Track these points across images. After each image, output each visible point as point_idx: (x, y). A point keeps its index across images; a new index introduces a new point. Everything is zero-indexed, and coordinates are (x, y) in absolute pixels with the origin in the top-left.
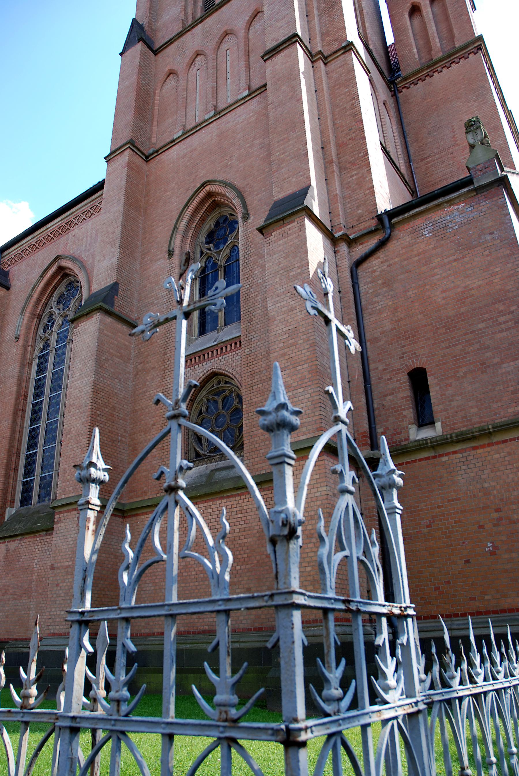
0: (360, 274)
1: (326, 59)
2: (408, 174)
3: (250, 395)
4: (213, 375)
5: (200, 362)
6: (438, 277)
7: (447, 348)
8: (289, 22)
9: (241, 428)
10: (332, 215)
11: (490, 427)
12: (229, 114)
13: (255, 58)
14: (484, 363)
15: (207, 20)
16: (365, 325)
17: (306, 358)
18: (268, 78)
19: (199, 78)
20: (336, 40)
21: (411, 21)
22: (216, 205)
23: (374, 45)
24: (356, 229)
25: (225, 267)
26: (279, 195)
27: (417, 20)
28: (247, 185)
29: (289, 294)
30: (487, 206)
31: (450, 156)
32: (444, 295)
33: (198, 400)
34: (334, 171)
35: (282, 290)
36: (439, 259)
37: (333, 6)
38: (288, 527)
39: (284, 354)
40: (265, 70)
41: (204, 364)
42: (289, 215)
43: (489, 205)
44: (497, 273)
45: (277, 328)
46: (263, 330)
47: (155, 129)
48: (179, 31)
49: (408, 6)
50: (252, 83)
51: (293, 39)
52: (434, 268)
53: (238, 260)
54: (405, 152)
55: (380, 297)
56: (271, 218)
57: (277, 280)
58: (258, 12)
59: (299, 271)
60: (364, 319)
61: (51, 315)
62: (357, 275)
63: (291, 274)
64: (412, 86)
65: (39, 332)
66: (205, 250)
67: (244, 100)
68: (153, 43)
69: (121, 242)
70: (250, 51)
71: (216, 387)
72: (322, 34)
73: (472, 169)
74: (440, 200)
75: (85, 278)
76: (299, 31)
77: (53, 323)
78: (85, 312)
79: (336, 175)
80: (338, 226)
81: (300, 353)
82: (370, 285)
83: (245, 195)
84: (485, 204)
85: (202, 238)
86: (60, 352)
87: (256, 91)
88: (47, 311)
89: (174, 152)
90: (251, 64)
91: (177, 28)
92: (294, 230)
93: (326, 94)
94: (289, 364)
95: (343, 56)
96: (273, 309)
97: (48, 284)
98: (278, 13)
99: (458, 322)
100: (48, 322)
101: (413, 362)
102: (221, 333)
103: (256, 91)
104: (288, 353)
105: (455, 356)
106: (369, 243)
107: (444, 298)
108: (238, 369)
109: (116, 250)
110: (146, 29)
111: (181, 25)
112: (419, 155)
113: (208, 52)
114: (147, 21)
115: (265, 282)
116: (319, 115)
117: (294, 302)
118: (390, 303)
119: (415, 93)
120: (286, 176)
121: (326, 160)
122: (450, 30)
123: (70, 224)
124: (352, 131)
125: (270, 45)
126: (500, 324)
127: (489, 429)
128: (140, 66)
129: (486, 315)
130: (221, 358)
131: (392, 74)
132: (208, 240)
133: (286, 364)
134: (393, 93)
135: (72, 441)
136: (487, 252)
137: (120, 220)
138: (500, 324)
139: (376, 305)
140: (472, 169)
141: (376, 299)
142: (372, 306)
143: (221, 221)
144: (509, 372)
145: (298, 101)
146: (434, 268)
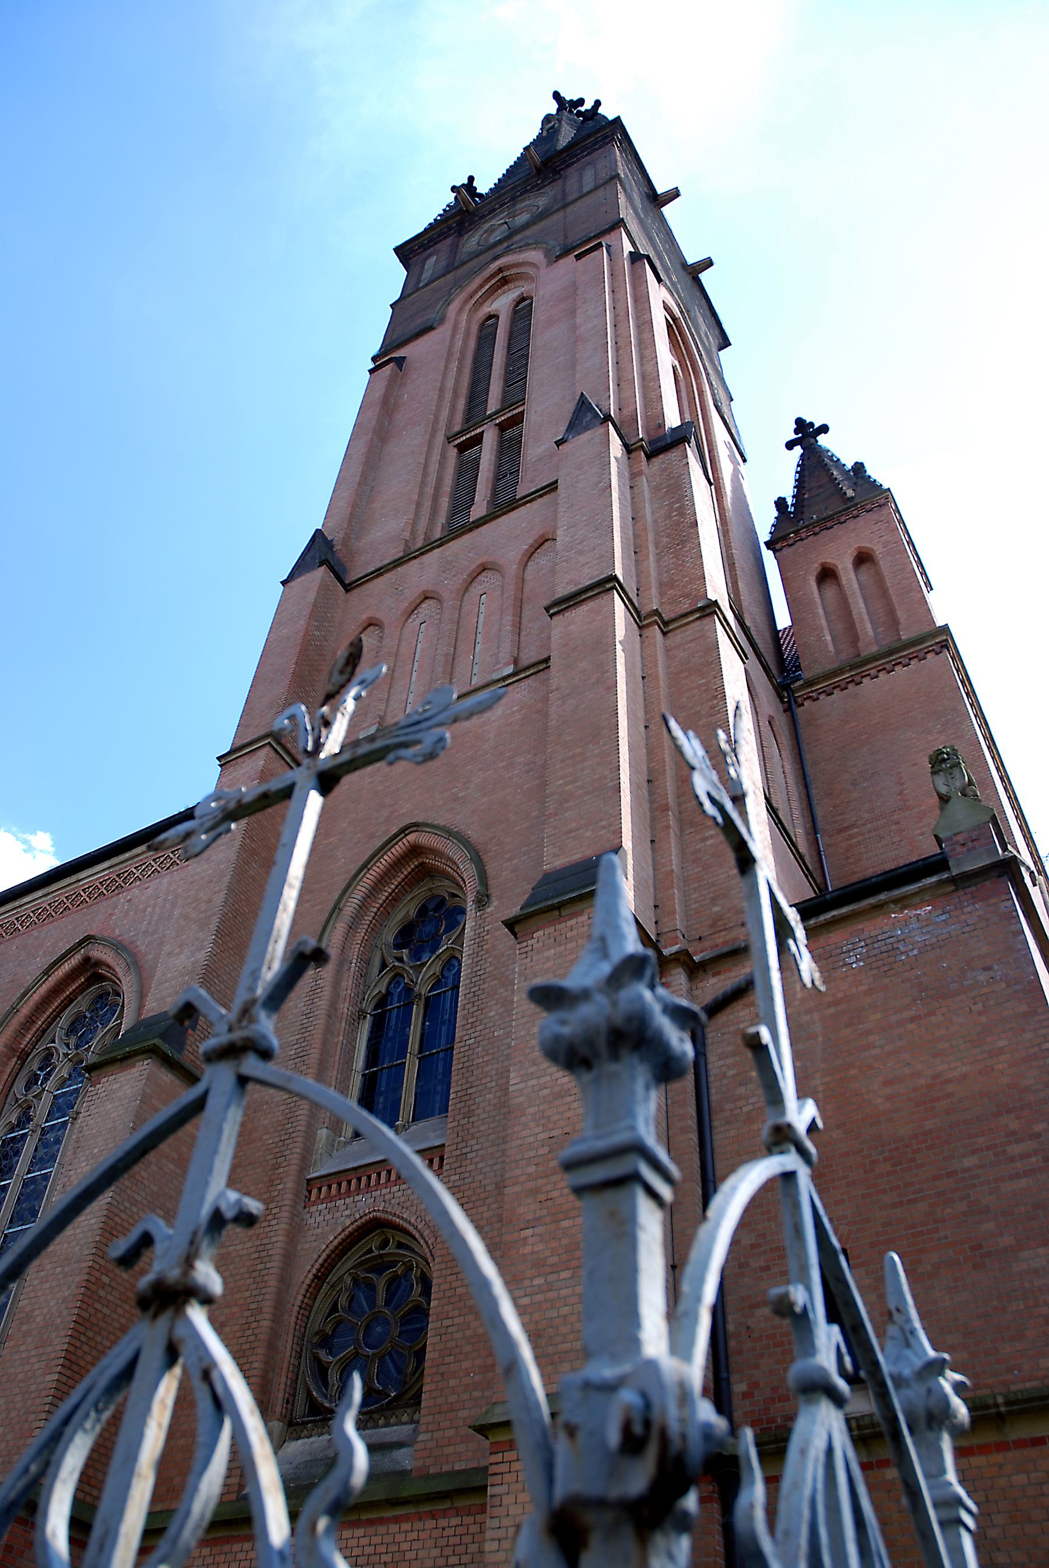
0: (709, 1035)
1: (666, 626)
2: (811, 856)
3: (449, 1279)
4: (374, 1225)
5: (349, 1193)
6: (877, 1051)
7: (894, 1206)
8: (601, 556)
9: (420, 1355)
10: (659, 911)
11: (1000, 1400)
13: (533, 611)
14: (980, 1247)
15: (450, 544)
16: (716, 1144)
18: (553, 646)
19: (423, 636)
20: (686, 596)
21: (820, 591)
22: (425, 873)
23: (754, 621)
24: (707, 944)
25: (427, 999)
26: (555, 860)
27: (830, 591)
28: (494, 838)
30: (977, 913)
31: (894, 827)
32: (889, 1090)
33: (332, 1278)
34: (668, 827)
36: (879, 1015)
37: (683, 543)
38: (652, 1451)
39: (537, 1191)
40: (549, 633)
41: (357, 1198)
42: (572, 901)
43: (981, 913)
44: (1001, 1051)
45: (524, 1133)
46: (492, 1137)
48: (396, 557)
49: (816, 567)
50: (521, 655)
51: (608, 583)
52: (869, 1033)
53: (456, 987)
54: (807, 813)
56: (536, 904)
58: (547, 540)
60: (715, 1131)
61: (49, 1055)
62: (704, 1038)
64: (822, 697)
65: (15, 1089)
66: (390, 960)
69: (222, 922)
70: (525, 599)
71: (376, 1253)
72: (661, 584)
73: (946, 841)
74: (883, 897)
75: (135, 988)
76: (619, 572)
77: (49, 1074)
78: (119, 1054)
79: (672, 835)
80: (672, 934)
82: (731, 1060)
83: (486, 858)
84: (973, 910)
85: (389, 935)
86: (51, 1137)
87: (528, 668)
88: (41, 1047)
90: (524, 621)
92: (581, 930)
93: (662, 684)
95: (698, 623)
96: (521, 1090)
97: (56, 990)
98: (583, 541)
99: (919, 1150)
100: (40, 1069)
103: (528, 668)
105: (914, 1226)
106: (732, 974)
107: (888, 1098)
109: (208, 938)
110: (337, 548)
111: (402, 547)
112: (835, 822)
113: (445, 594)
114: (341, 536)
115: (508, 1035)
116: (647, 720)
119: (828, 710)
120: (574, 825)
121: (655, 805)
122: (891, 612)
123: (126, 878)
125: (563, 590)
126: (1012, 1159)
127: (996, 1405)
128: (315, 605)
129: (981, 1140)
130: (396, 1188)
131: (784, 673)
132: (400, 941)
133: (539, 1213)
134: (786, 705)
135: (29, 1339)
136: (979, 1007)
137: (227, 878)
138: (1012, 1159)
140: (946, 841)
141: (741, 1091)
142: (733, 1106)
143: (431, 907)
144: (1036, 1271)
145: (608, 689)
146: (869, 1033)
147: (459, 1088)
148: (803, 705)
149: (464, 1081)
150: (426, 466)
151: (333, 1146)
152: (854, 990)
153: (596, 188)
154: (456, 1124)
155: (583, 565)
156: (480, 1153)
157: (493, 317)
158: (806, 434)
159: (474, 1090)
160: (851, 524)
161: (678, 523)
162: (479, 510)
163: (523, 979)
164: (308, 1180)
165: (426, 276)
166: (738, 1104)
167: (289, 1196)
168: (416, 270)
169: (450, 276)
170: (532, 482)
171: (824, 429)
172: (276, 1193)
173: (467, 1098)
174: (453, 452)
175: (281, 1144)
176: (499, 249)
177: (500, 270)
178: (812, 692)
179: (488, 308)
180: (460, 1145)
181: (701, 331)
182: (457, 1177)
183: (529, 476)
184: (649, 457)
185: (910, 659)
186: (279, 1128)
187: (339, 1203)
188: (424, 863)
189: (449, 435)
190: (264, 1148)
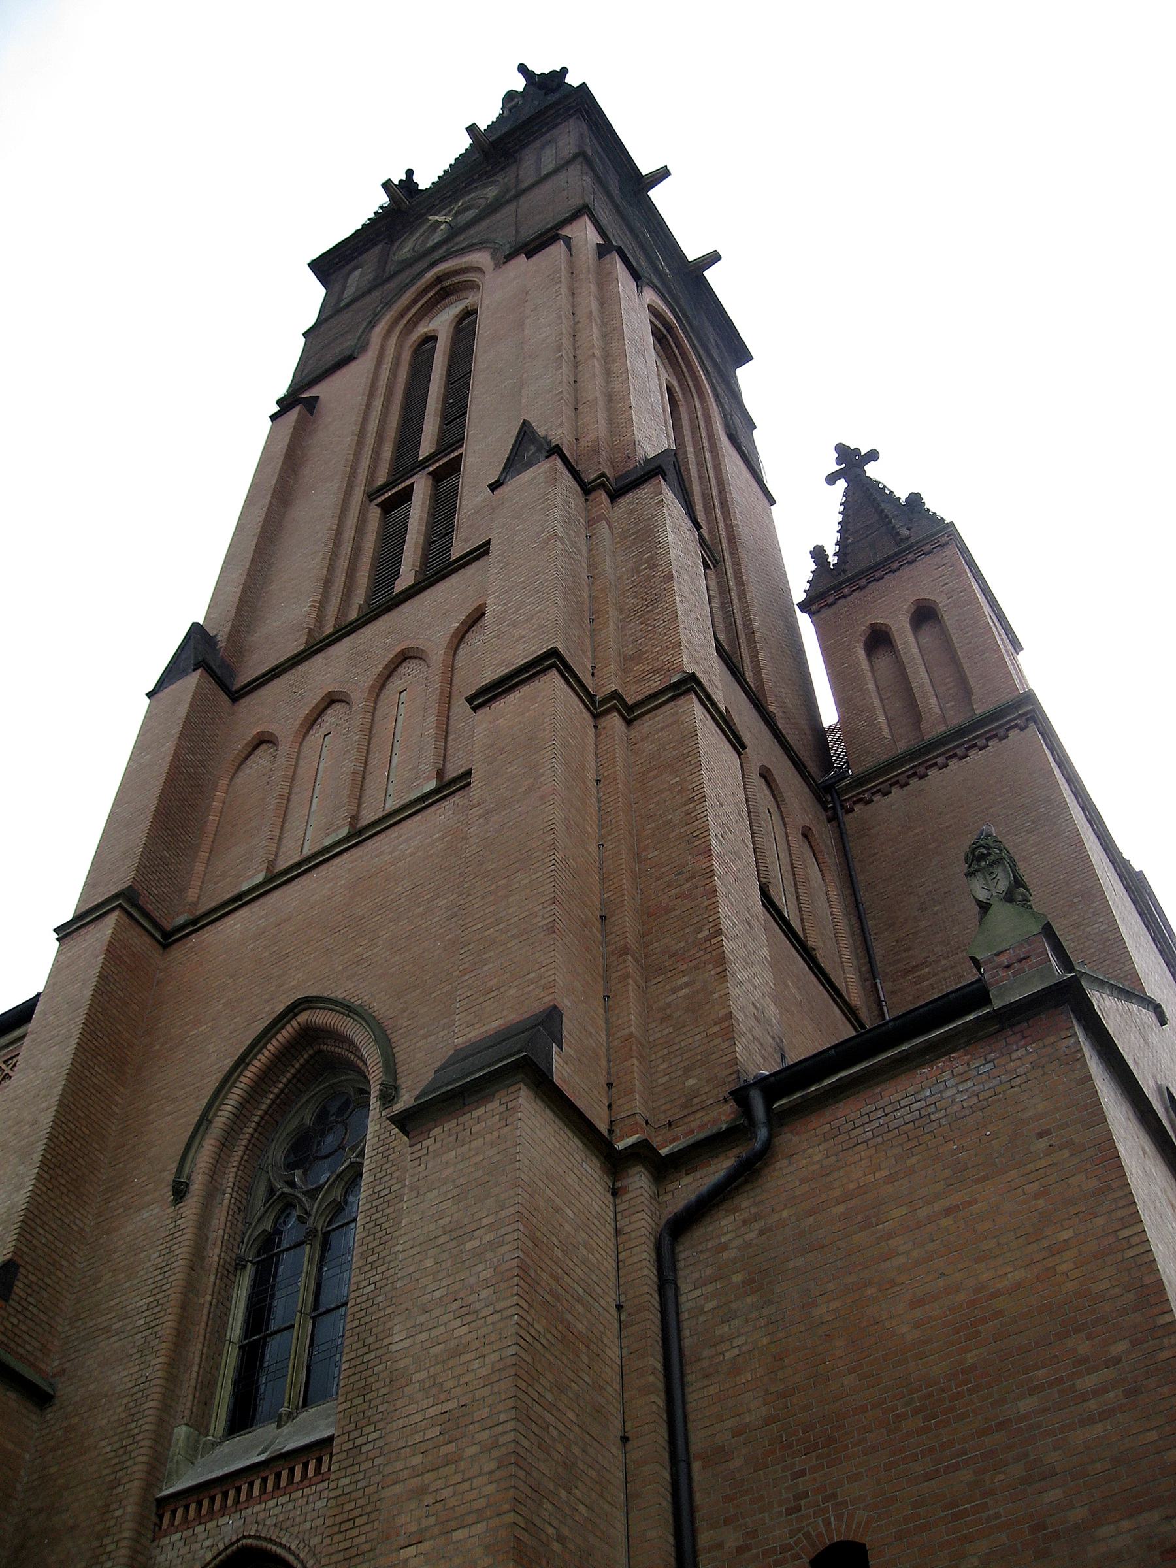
1: (631, 713)
6: (902, 1260)
7: (928, 1477)
12: (383, 835)
16: (690, 1407)
17: (482, 1502)
19: (331, 752)
20: (657, 671)
21: (870, 661)
24: (679, 1130)
27: (884, 661)
29: (456, 1305)
32: (918, 1313)
35: (437, 1294)
36: (904, 1210)
37: (654, 602)
39: (422, 1491)
41: (222, 1521)
45: (413, 1408)
47: (200, 867)
50: (448, 765)
52: (890, 1236)
55: (735, 1322)
57: (429, 1263)
59: (490, 1237)
60: (688, 1390)
62: (674, 1261)
63: (468, 1246)
67: (424, 803)
68: (233, 674)
69: (48, 1149)
81: (466, 1486)
82: (710, 1288)
83: (395, 1037)
84: (1021, 1056)
85: (277, 1154)
89: (235, 925)
90: (451, 722)
91: (296, 645)
94: (432, 1520)
101: (827, 1524)
102: (285, 1430)
104: (433, 1487)
106: (711, 1169)
108: (315, 1541)
112: (899, 961)
114: (227, 630)
116: (602, 837)
117: (465, 1329)
118: (765, 1341)
121: (610, 948)
124: (684, 876)
126: (1084, 1398)
128: (187, 721)
130: (272, 1503)
132: (292, 1159)
133: (425, 1523)
137: (59, 1089)
138: (1084, 1398)
139: (722, 1347)
147: (353, 1355)
148: (852, 810)
149: (360, 1344)
150: (339, 532)
151: (196, 1449)
152: (870, 1178)
153: (556, 171)
154: (348, 1404)
155: (517, 640)
156: (379, 1443)
157: (431, 339)
158: (851, 463)
159: (372, 1355)
160: (906, 571)
161: (648, 579)
162: (406, 578)
163: (414, 1194)
164: (162, 1502)
165: (349, 292)
166: (719, 1348)
167: (128, 1525)
168: (337, 287)
169: (376, 294)
170: (466, 540)
171: (873, 455)
172: (112, 1522)
173: (364, 1366)
174: (375, 513)
175: (121, 1451)
176: (437, 255)
177: (439, 279)
178: (864, 792)
179: (422, 329)
180: (353, 1435)
181: (700, 337)
182: (348, 1480)
183: (462, 535)
184: (614, 497)
185: (988, 739)
186: (120, 1430)
187: (199, 1529)
188: (321, 1051)
189: (371, 490)
190: (100, 1459)
